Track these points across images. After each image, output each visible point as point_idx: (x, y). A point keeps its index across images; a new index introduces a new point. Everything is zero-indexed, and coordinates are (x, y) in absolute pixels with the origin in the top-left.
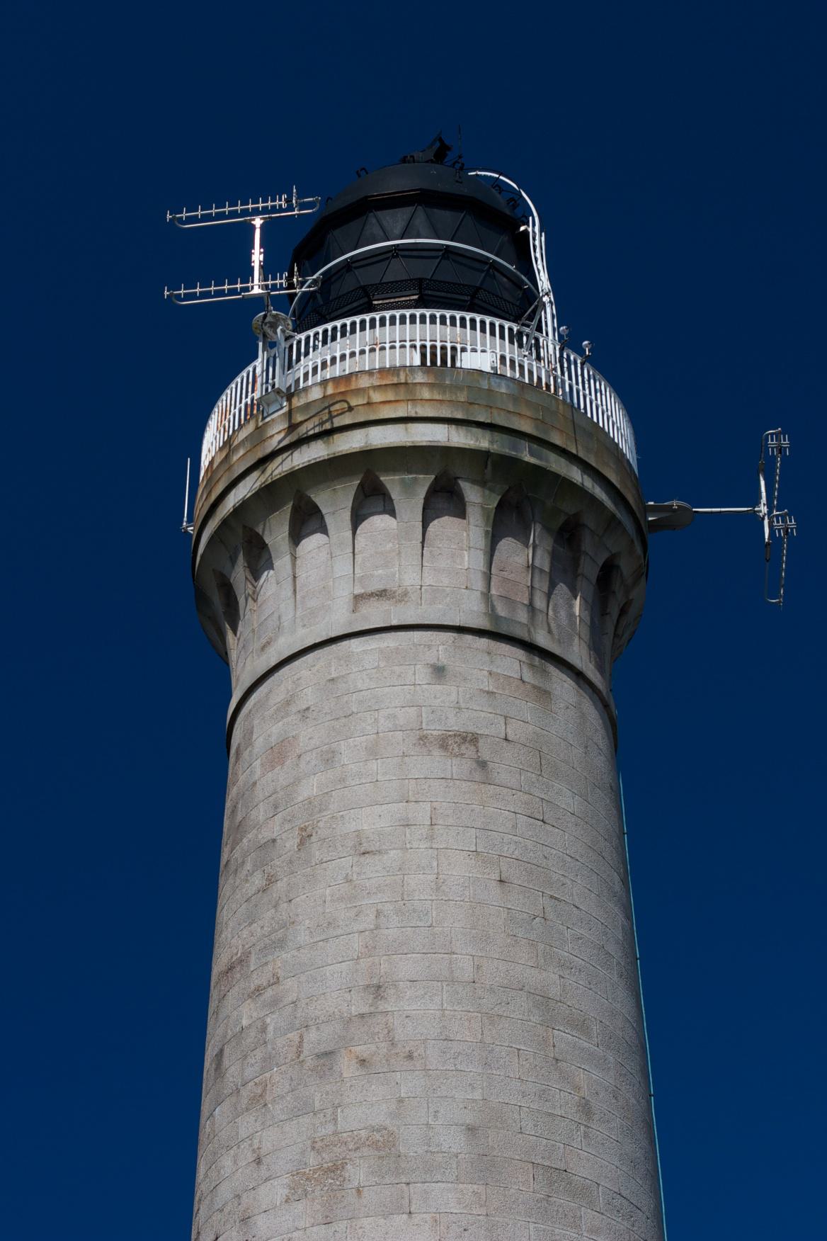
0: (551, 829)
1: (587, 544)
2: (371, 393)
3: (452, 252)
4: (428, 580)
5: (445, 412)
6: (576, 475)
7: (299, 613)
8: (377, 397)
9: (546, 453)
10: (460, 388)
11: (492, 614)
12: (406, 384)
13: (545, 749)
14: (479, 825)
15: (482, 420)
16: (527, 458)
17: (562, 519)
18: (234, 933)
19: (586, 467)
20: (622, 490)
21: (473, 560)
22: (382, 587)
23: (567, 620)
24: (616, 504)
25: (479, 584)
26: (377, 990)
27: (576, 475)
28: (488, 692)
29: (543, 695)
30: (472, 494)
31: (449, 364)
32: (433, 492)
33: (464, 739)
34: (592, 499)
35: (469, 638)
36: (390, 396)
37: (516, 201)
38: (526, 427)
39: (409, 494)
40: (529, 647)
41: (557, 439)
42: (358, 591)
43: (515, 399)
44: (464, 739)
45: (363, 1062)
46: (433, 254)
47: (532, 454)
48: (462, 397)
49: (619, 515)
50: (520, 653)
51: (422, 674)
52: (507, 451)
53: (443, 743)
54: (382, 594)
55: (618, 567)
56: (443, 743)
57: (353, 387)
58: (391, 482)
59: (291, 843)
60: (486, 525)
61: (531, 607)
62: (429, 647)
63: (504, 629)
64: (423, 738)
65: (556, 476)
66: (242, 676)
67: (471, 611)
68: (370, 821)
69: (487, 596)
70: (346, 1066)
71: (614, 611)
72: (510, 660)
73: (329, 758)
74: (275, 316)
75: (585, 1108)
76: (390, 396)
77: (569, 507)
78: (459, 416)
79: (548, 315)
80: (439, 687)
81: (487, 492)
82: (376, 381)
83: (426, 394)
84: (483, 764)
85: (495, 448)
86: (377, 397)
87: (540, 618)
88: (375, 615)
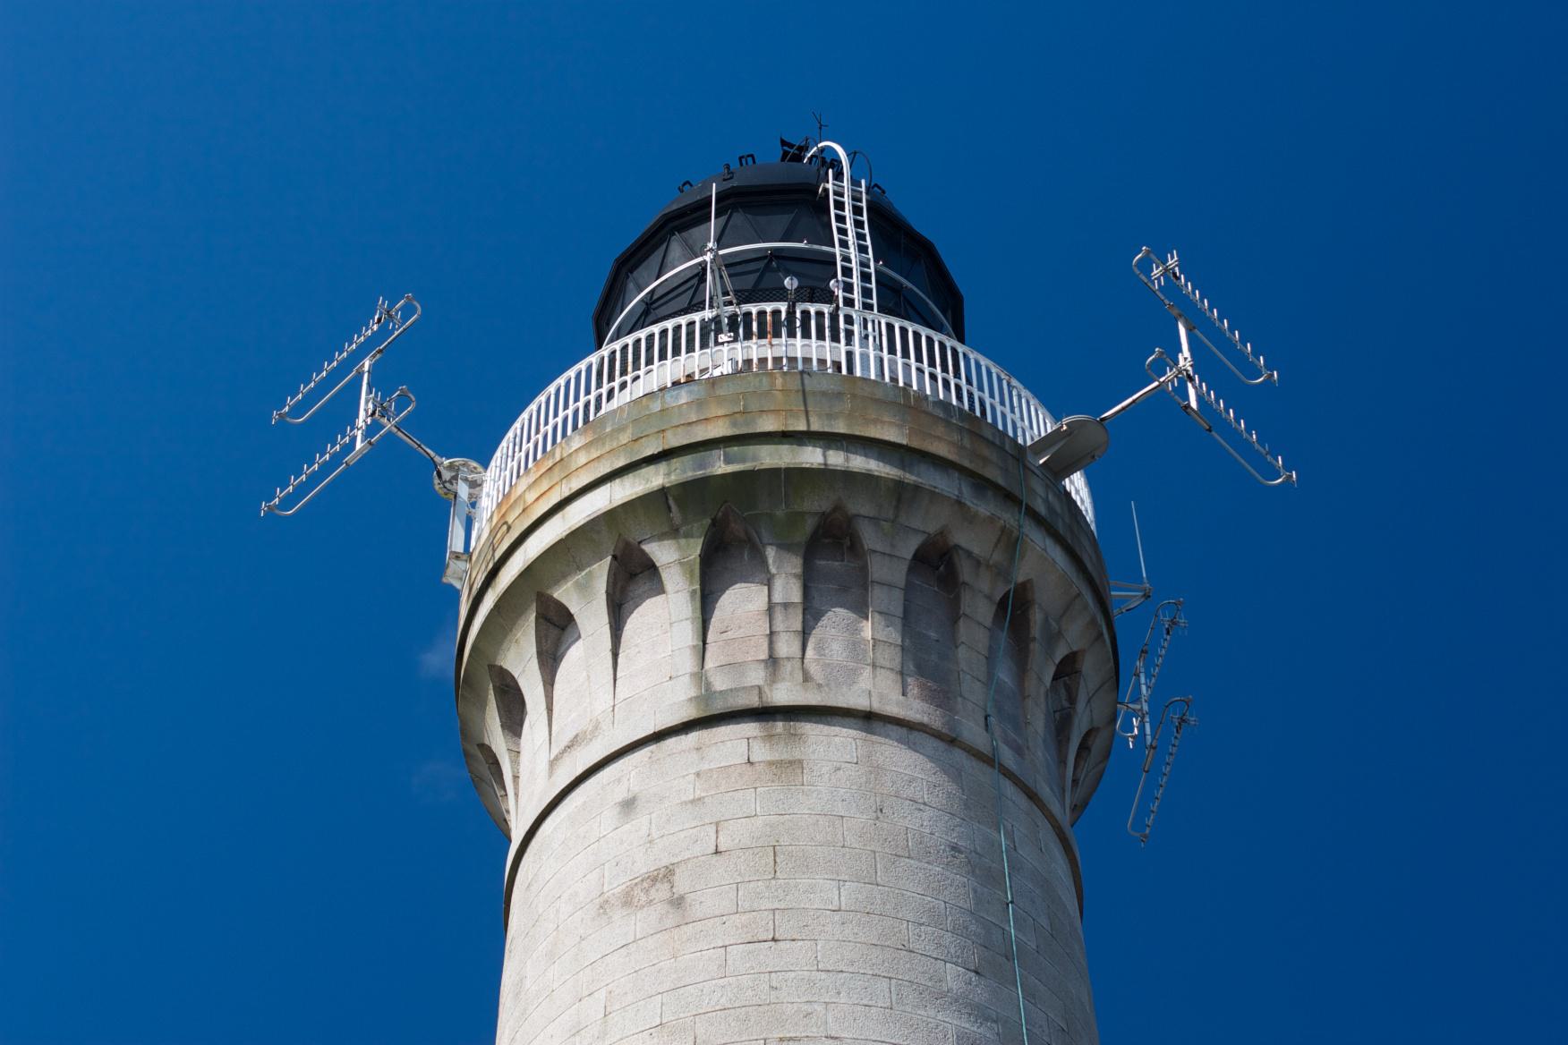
0: (788, 945)
1: (870, 538)
3: (778, 257)
6: (812, 456)
10: (621, 429)
13: (785, 840)
14: (667, 986)
17: (810, 525)
19: (828, 440)
20: (915, 444)
23: (856, 655)
24: (903, 467)
27: (812, 456)
28: (692, 802)
30: (663, 553)
33: (654, 880)
34: (848, 476)
35: (671, 743)
37: (822, 150)
44: (654, 880)
46: (752, 266)
47: (728, 461)
49: (910, 478)
50: (750, 728)
52: (690, 474)
53: (627, 900)
55: (957, 547)
56: (627, 900)
58: (565, 593)
60: (691, 583)
62: (619, 780)
65: (774, 473)
72: (733, 741)
74: (451, 467)
76: (545, 486)
77: (816, 503)
78: (621, 463)
80: (628, 826)
81: (683, 541)
85: (675, 478)
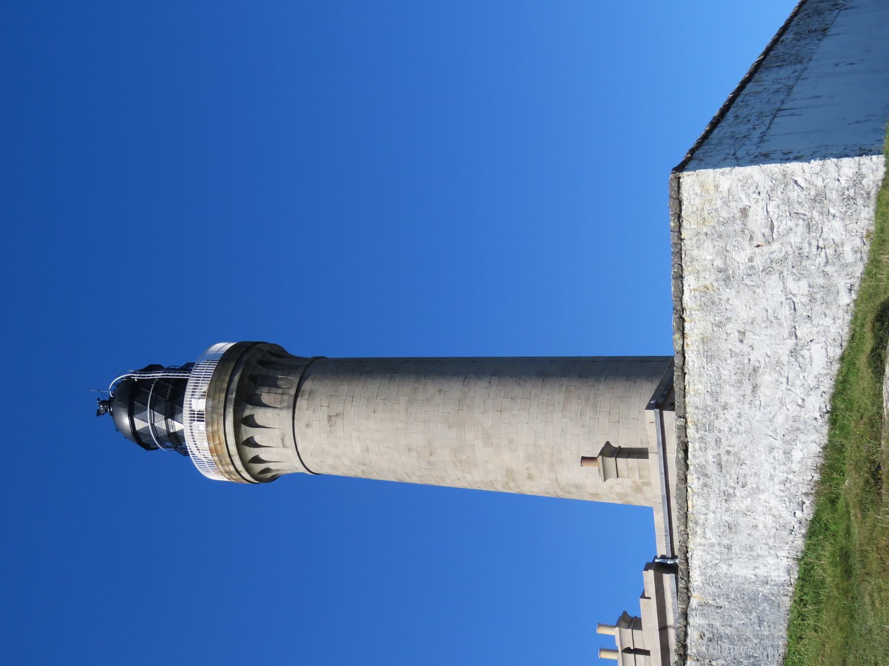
11: (288, 407)
16: (234, 396)
18: (391, 478)
21: (269, 412)
25: (277, 411)
26: (410, 449)
29: (311, 393)
30: (247, 413)
36: (217, 438)
38: (223, 396)
39: (248, 432)
40: (296, 396)
41: (225, 386)
43: (214, 399)
45: (431, 454)
48: (215, 416)
50: (299, 399)
51: (309, 431)
52: (233, 403)
54: (282, 440)
59: (364, 467)
61: (283, 394)
63: (292, 404)
64: (330, 431)
66: (302, 470)
67: (287, 414)
68: (357, 448)
69: (281, 409)
70: (432, 459)
71: (274, 359)
73: (337, 457)
75: (440, 391)
76: (217, 438)
82: (212, 442)
83: (215, 428)
84: (337, 415)
86: (217, 442)
87: (285, 391)
88: (290, 442)
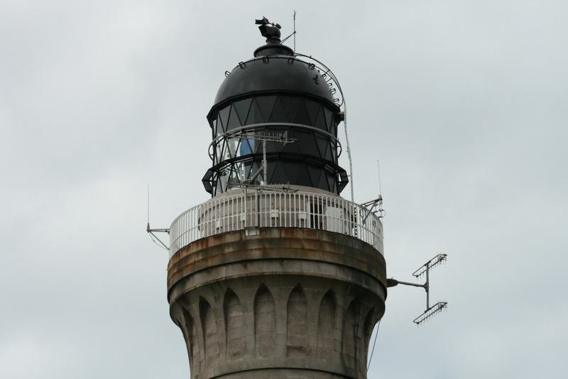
2: (304, 242)
4: (320, 346)
5: (336, 261)
7: (257, 346)
8: (307, 246)
9: (372, 282)
12: (319, 241)
15: (349, 265)
22: (300, 345)
31: (319, 228)
32: (294, 291)
42: (289, 344)
54: (300, 349)
57: (295, 237)
58: (238, 291)
79: (265, 160)
83: (328, 248)
86: (307, 246)
